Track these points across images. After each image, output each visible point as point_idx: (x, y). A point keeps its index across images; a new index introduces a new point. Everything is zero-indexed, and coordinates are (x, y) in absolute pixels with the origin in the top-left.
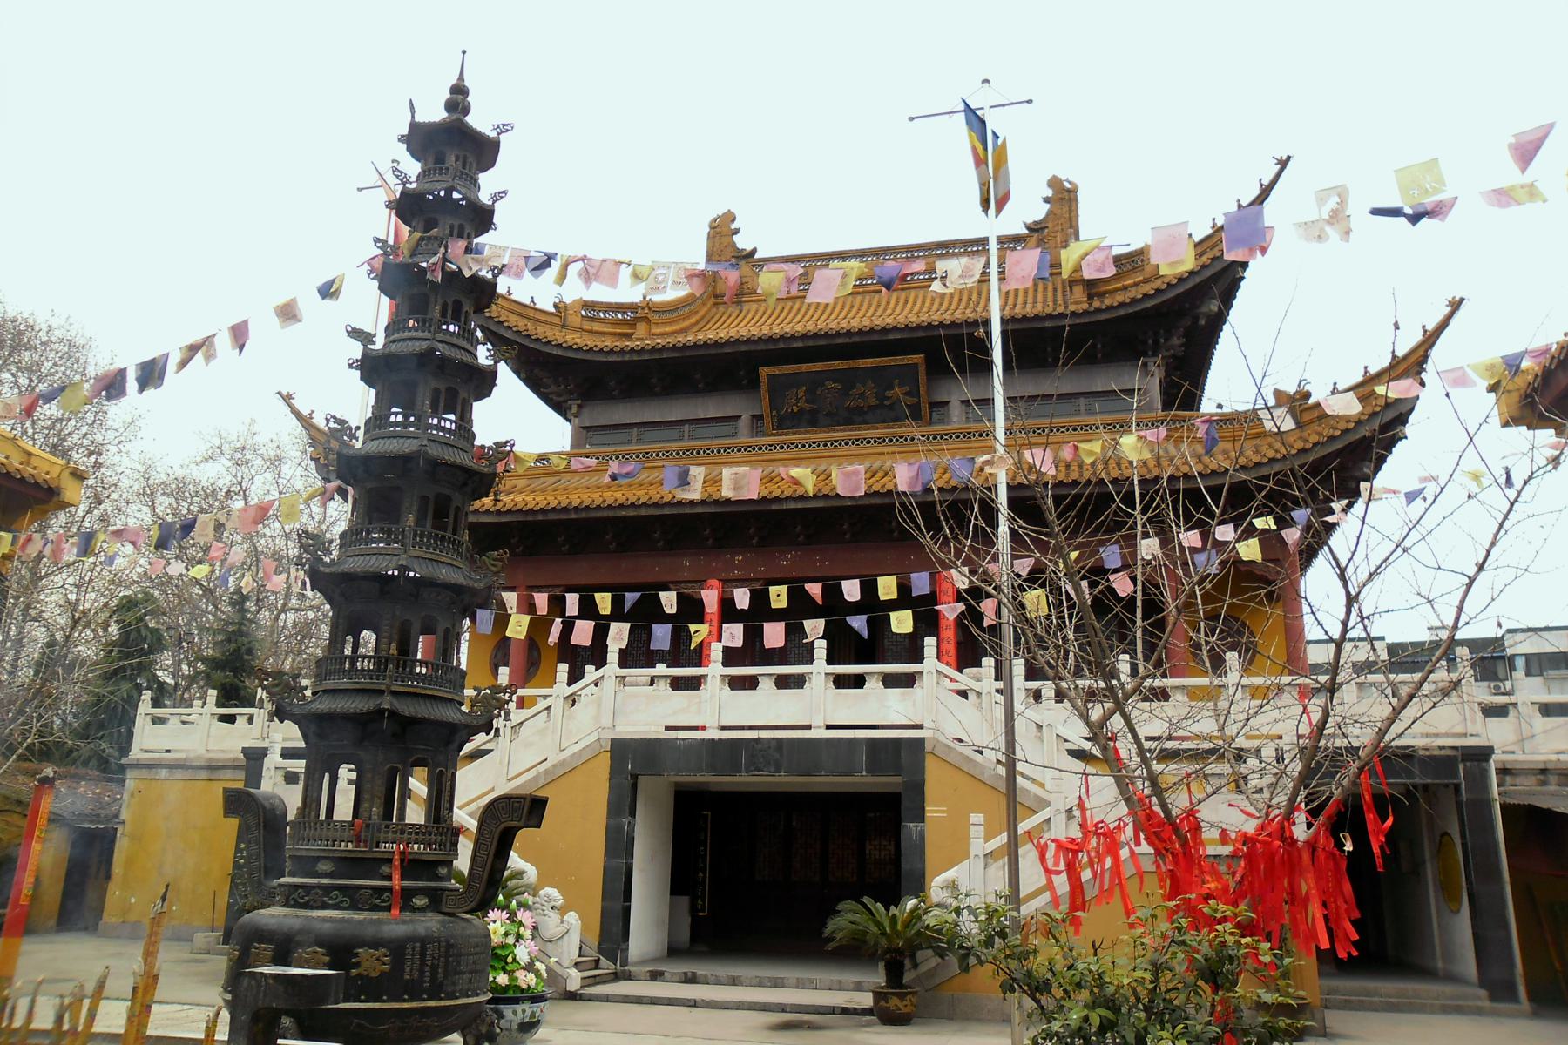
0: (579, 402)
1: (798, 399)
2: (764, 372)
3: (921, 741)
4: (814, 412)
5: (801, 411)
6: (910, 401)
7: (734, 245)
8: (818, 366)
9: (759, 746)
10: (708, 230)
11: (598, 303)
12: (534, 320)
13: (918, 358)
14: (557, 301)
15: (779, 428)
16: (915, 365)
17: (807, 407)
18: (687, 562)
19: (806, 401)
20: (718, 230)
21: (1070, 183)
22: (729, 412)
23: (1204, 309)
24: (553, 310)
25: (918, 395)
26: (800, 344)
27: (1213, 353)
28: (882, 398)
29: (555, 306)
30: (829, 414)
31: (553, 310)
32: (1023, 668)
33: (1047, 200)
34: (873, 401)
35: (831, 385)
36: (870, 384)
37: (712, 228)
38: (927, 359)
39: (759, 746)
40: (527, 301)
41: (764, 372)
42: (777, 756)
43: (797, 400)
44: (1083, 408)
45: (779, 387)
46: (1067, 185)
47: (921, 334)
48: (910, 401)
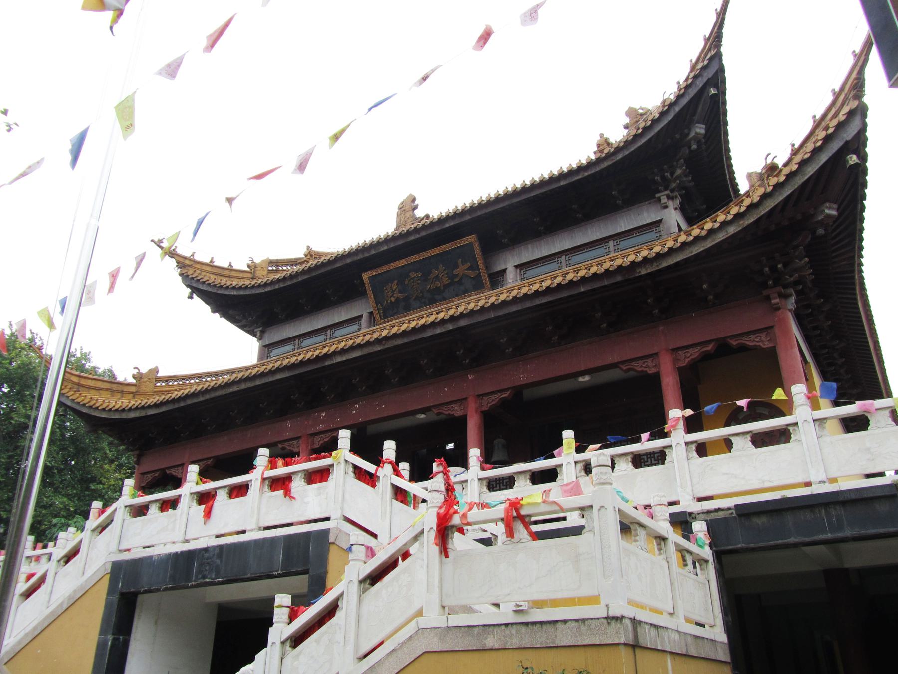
0: (261, 328)
1: (393, 292)
2: (366, 276)
3: (326, 532)
4: (406, 299)
5: (397, 299)
6: (472, 274)
7: (414, 215)
8: (402, 263)
9: (206, 555)
10: (397, 210)
11: (281, 260)
12: (229, 277)
13: (472, 238)
14: (250, 262)
15: (385, 317)
16: (471, 244)
17: (400, 295)
18: (289, 424)
19: (400, 292)
20: (403, 209)
21: (642, 109)
22: (355, 314)
23: (692, 134)
24: (247, 269)
25: (478, 268)
26: (385, 248)
27: (861, 264)
28: (452, 277)
29: (249, 266)
30: (417, 298)
31: (247, 269)
32: (349, 442)
33: (626, 127)
34: (446, 280)
35: (413, 275)
36: (441, 266)
37: (400, 208)
38: (481, 239)
39: (206, 555)
40: (226, 265)
41: (366, 276)
42: (218, 561)
43: (393, 293)
44: (612, 248)
45: (379, 284)
46: (640, 111)
47: (468, 217)
48: (472, 274)
